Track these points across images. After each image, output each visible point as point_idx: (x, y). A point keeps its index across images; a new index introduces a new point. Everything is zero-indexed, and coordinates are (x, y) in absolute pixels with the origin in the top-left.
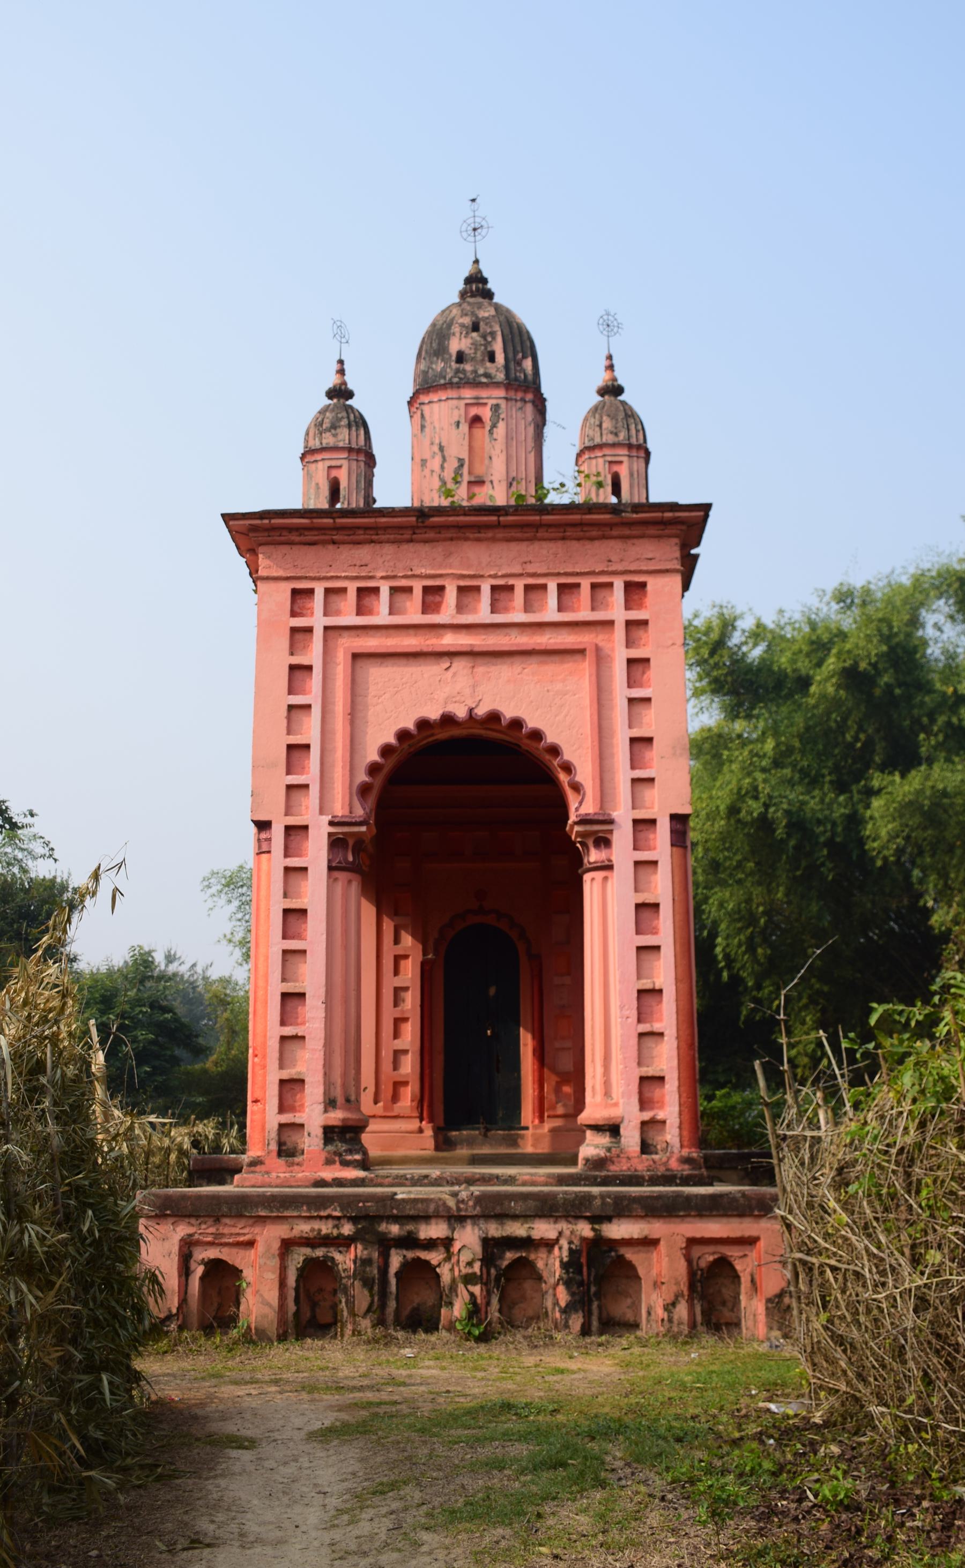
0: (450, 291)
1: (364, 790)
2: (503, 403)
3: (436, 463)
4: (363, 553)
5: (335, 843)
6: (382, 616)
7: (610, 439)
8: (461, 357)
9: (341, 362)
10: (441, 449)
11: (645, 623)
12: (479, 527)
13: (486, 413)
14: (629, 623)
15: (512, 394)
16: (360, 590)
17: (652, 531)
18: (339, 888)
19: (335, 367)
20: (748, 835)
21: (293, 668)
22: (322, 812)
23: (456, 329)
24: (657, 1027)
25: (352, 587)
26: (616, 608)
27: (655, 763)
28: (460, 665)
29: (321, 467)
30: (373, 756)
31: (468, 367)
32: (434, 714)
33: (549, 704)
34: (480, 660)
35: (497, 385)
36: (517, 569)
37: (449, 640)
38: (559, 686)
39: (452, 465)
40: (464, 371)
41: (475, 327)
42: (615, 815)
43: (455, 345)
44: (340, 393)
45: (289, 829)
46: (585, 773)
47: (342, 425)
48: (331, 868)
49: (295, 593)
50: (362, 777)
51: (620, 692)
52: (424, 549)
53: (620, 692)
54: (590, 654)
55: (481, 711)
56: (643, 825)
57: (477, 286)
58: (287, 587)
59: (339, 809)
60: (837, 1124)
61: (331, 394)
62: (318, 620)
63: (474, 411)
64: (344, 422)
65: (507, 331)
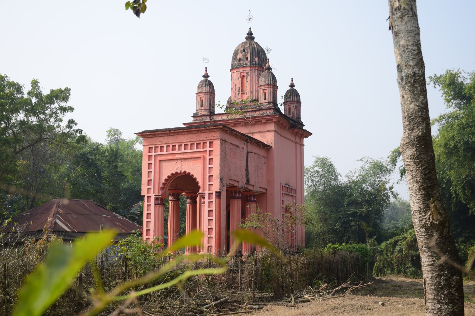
0: (243, 39)
1: (162, 188)
2: (249, 71)
3: (234, 89)
4: (161, 139)
5: (156, 199)
6: (165, 152)
7: (264, 83)
8: (240, 60)
9: (206, 68)
10: (235, 85)
11: (213, 150)
12: (181, 132)
13: (245, 74)
14: (210, 151)
15: (252, 68)
16: (161, 147)
17: (214, 130)
18: (157, 208)
19: (205, 69)
21: (149, 164)
22: (154, 193)
23: (239, 52)
24: (211, 236)
25: (159, 146)
26: (208, 149)
27: (214, 181)
28: (179, 161)
29: (199, 97)
30: (163, 181)
31: (241, 62)
32: (174, 172)
33: (194, 169)
34: (183, 160)
35: (248, 66)
36: (189, 140)
37: (177, 156)
38: (197, 165)
39: (237, 89)
40: (240, 64)
41: (244, 51)
42: (205, 192)
43: (239, 56)
44: (206, 76)
45: (148, 197)
46: (200, 184)
47: (207, 88)
48: (155, 205)
49: (150, 148)
50: (161, 186)
51: (208, 166)
52: (172, 137)
53: (208, 166)
54: (202, 158)
55: (182, 171)
56: (210, 194)
57: (250, 36)
58: (148, 147)
59: (157, 193)
61: (204, 76)
62: (153, 154)
63: (243, 74)
64: (204, 85)
65: (251, 51)
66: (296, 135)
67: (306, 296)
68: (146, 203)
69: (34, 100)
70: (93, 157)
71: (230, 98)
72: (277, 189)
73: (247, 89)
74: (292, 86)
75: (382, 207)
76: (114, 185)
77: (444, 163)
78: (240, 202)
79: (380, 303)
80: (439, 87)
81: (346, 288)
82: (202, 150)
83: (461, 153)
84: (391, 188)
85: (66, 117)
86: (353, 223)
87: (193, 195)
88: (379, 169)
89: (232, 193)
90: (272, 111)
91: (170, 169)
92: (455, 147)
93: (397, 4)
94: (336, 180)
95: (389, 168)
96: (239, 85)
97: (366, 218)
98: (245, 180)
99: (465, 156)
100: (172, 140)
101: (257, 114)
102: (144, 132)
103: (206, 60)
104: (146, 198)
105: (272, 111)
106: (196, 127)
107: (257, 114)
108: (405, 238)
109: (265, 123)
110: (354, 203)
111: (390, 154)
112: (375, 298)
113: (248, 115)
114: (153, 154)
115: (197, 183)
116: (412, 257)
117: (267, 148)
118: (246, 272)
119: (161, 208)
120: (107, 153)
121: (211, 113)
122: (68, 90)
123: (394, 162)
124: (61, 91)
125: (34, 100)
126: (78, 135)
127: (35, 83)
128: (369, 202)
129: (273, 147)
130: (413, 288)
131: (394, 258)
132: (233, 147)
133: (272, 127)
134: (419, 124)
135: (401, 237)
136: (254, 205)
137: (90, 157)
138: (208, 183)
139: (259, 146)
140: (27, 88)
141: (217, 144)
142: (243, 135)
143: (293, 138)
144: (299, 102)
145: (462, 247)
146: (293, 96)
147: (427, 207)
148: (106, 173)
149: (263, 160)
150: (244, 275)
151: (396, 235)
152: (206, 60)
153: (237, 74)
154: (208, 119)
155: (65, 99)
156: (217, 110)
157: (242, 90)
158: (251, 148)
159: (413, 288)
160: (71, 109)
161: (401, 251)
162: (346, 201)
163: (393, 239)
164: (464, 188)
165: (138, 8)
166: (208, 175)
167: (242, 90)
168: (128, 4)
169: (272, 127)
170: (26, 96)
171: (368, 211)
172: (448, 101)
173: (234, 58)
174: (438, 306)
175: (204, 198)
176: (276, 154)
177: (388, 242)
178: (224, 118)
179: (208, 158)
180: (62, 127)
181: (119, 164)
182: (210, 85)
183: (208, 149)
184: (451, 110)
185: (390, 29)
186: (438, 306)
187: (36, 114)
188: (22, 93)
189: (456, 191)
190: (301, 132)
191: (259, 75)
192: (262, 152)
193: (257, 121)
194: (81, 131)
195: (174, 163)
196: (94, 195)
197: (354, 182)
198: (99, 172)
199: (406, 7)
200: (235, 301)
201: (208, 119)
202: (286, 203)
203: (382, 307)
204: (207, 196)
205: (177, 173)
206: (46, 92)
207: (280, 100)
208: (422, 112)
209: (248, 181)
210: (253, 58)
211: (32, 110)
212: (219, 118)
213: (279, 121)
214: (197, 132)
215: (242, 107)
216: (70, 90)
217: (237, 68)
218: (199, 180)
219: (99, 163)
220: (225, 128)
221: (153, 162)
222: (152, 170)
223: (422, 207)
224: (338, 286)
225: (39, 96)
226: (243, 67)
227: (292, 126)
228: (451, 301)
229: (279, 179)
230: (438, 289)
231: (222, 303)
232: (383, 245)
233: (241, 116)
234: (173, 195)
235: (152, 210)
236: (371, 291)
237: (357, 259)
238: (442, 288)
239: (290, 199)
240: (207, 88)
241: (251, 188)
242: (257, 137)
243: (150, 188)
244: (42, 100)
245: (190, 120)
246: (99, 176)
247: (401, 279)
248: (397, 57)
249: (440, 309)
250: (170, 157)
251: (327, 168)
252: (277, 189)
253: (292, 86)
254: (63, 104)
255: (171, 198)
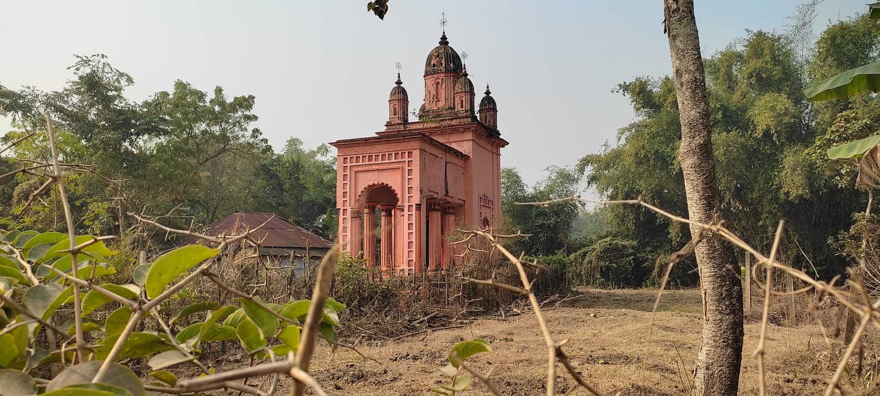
6: (361, 163)
13: (440, 81)
26: (407, 159)
28: (376, 173)
33: (393, 180)
37: (374, 167)
44: (399, 83)
46: (399, 196)
47: (400, 95)
51: (407, 177)
53: (407, 177)
57: (444, 41)
62: (349, 165)
66: (493, 144)
67: (515, 310)
68: (341, 217)
69: (217, 108)
70: (274, 168)
71: (424, 106)
73: (442, 96)
74: (488, 93)
76: (296, 198)
77: (633, 173)
78: (439, 214)
79: (592, 315)
80: (628, 96)
81: (555, 301)
83: (652, 162)
85: (251, 126)
86: (541, 235)
87: (388, 207)
88: (566, 178)
89: (431, 205)
90: (469, 120)
91: (367, 180)
92: (646, 156)
93: (674, 6)
94: (522, 190)
95: (576, 176)
96: (433, 92)
98: (444, 192)
101: (454, 122)
102: (338, 142)
104: (341, 211)
105: (469, 120)
107: (454, 122)
108: (594, 249)
109: (463, 132)
110: (542, 213)
112: (587, 310)
113: (444, 123)
114: (349, 165)
115: (396, 195)
116: (601, 268)
117: (464, 157)
118: (454, 286)
120: (287, 165)
121: (405, 121)
122: (252, 98)
123: (582, 170)
124: (244, 98)
125: (217, 108)
126: (264, 144)
127: (219, 91)
128: (557, 214)
129: (471, 155)
130: (612, 298)
133: (469, 136)
135: (591, 248)
136: (453, 218)
137: (271, 168)
138: (407, 195)
139: (457, 156)
140: (211, 96)
141: (416, 154)
142: (442, 144)
143: (489, 148)
144: (495, 110)
146: (489, 103)
148: (287, 186)
149: (462, 171)
150: (451, 290)
151: (585, 246)
153: (431, 81)
154: (402, 128)
155: (249, 107)
156: (412, 118)
157: (437, 97)
158: (453, 159)
159: (612, 298)
160: (255, 118)
161: (590, 262)
162: (534, 213)
163: (582, 251)
165: (380, 8)
167: (437, 97)
168: (370, 6)
169: (469, 136)
170: (208, 104)
171: (557, 222)
172: (638, 109)
174: (719, 317)
176: (474, 162)
177: (578, 253)
179: (407, 168)
180: (246, 136)
181: (301, 176)
182: (404, 92)
183: (407, 159)
184: (641, 118)
185: (665, 31)
186: (719, 317)
188: (204, 102)
190: (498, 141)
191: (455, 83)
192: (460, 162)
194: (266, 141)
195: (371, 174)
197: (541, 192)
198: (280, 185)
199: (685, 9)
200: (444, 316)
201: (402, 128)
202: (483, 216)
203: (595, 319)
204: (406, 209)
205: (374, 185)
206: (229, 100)
207: (477, 108)
208: (703, 119)
209: (447, 192)
210: (447, 64)
211: (216, 119)
212: (414, 127)
214: (395, 141)
215: (438, 115)
216: (254, 97)
217: (431, 74)
218: (398, 192)
219: (280, 175)
220: (424, 137)
222: (348, 182)
224: (546, 299)
225: (222, 104)
227: (490, 136)
228: (733, 312)
231: (432, 318)
232: (572, 256)
233: (437, 125)
234: (369, 207)
236: (573, 304)
237: (556, 271)
238: (723, 299)
239: (487, 210)
240: (400, 95)
241: (450, 200)
242: (454, 146)
243: (346, 200)
245: (383, 129)
246: (281, 189)
247: (592, 290)
248: (674, 62)
249: (721, 320)
250: (366, 168)
251: (514, 179)
254: (247, 113)
255: (366, 211)
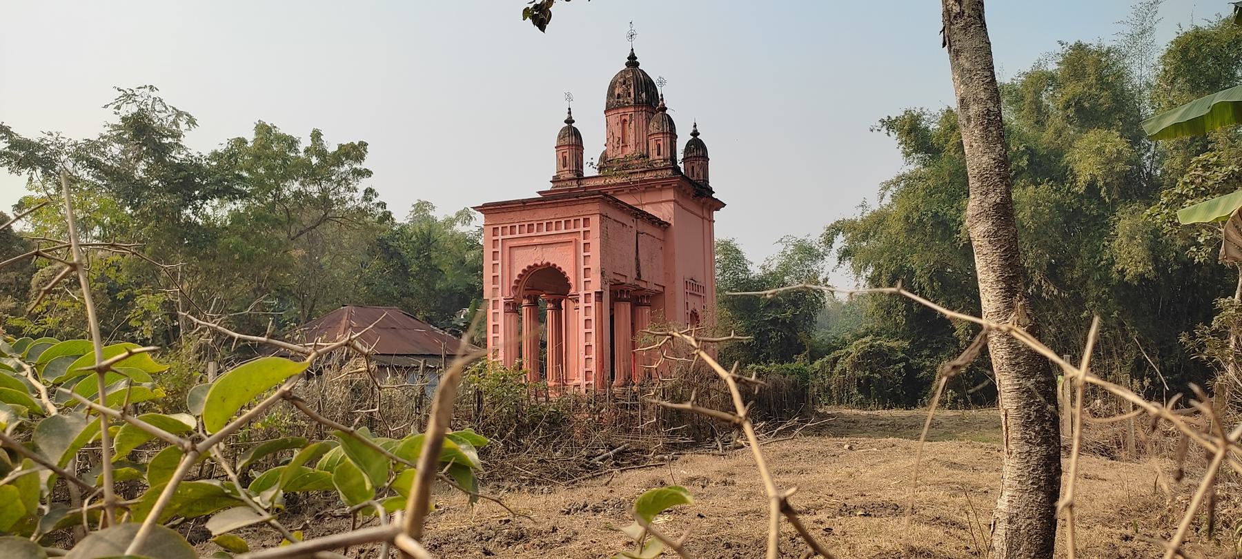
1: (515, 288)
5: (507, 304)
6: (517, 235)
13: (628, 118)
20: (845, 254)
26: (582, 229)
28: (539, 248)
33: (562, 259)
37: (536, 241)
44: (570, 121)
46: (572, 281)
47: (571, 138)
51: (583, 254)
57: (632, 61)
59: (507, 295)
60: (423, 394)
62: (500, 237)
66: (703, 206)
68: (490, 311)
69: (314, 160)
70: (395, 244)
71: (605, 153)
72: (679, 287)
73: (631, 139)
74: (695, 134)
75: (814, 309)
76: (427, 285)
77: (903, 245)
79: (846, 446)
81: (794, 428)
82: (572, 230)
84: (826, 280)
85: (363, 184)
86: (774, 334)
88: (807, 252)
90: (670, 172)
91: (525, 259)
92: (920, 221)
93: (957, 9)
94: (746, 271)
96: (618, 134)
97: (791, 326)
99: (933, 235)
100: (527, 216)
101: (648, 176)
102: (485, 205)
103: (569, 97)
105: (670, 172)
106: (554, 198)
107: (648, 176)
108: (849, 354)
109: (660, 190)
111: (824, 231)
113: (634, 178)
114: (500, 237)
115: (567, 279)
116: (859, 380)
117: (663, 225)
119: (514, 317)
120: (414, 238)
121: (579, 176)
122: (363, 145)
123: (829, 242)
124: (352, 146)
125: (314, 160)
126: (380, 210)
127: (316, 135)
128: (795, 303)
130: (874, 423)
131: (833, 382)
132: (617, 225)
133: (670, 195)
134: (995, 185)
135: (844, 351)
136: (647, 311)
138: (583, 280)
139: (653, 223)
140: (305, 142)
141: (595, 221)
142: (631, 207)
144: (705, 158)
145: (928, 363)
146: (697, 148)
147: (1010, 307)
148: (414, 268)
149: (660, 244)
151: (835, 349)
152: (569, 97)
153: (615, 118)
155: (360, 158)
156: (589, 171)
157: (623, 142)
159: (874, 423)
160: (368, 173)
161: (843, 372)
163: (832, 355)
164: (931, 279)
165: (540, 16)
166: (583, 267)
167: (623, 142)
169: (670, 195)
170: (302, 155)
172: (908, 155)
173: (611, 93)
174: (1027, 448)
175: (577, 301)
178: (598, 182)
179: (582, 242)
180: (356, 199)
181: (433, 255)
182: (577, 134)
183: (582, 229)
184: (912, 168)
185: (944, 45)
186: (1027, 448)
187: (315, 181)
188: (297, 151)
189: (920, 284)
191: (648, 120)
192: (656, 232)
193: (648, 187)
194: (383, 205)
195: (532, 250)
196: (399, 300)
197: (771, 274)
198: (404, 267)
200: (637, 450)
201: (575, 185)
204: (582, 299)
205: (536, 265)
206: (332, 148)
207: (680, 156)
209: (639, 274)
210: (637, 94)
211: (313, 175)
212: (592, 183)
213: (680, 187)
214: (566, 204)
216: (366, 144)
218: (570, 275)
219: (404, 253)
220: (606, 197)
221: (499, 249)
223: (1002, 306)
224: (780, 424)
225: (322, 154)
226: (624, 107)
227: (698, 194)
228: (1045, 441)
229: (683, 271)
230: (1027, 424)
231: (619, 453)
232: (817, 364)
233: (624, 180)
234: (529, 298)
235: (501, 321)
236: (819, 431)
237: (794, 385)
239: (697, 300)
240: (571, 138)
241: (643, 285)
242: (649, 209)
243: (496, 289)
244: (324, 160)
245: (548, 186)
246: (406, 273)
248: (957, 88)
249: (1029, 453)
250: (525, 242)
251: (734, 255)
252: (679, 287)
253: (695, 134)
254: (357, 166)
